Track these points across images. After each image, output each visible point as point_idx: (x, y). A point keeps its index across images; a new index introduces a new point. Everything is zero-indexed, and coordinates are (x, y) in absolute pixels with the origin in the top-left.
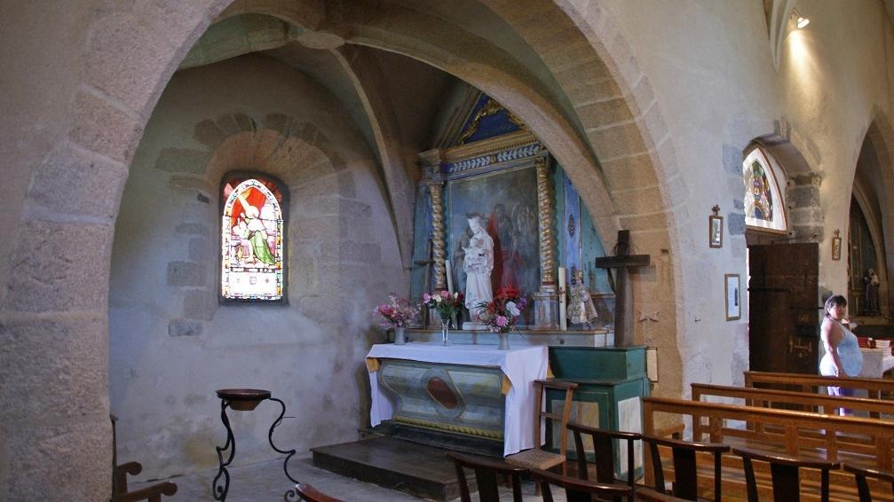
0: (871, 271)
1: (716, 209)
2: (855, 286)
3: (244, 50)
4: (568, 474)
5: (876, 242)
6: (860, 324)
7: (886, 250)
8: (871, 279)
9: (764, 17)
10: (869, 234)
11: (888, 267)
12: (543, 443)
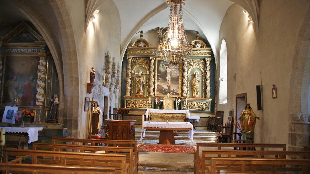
0: (55, 95)
1: (274, 86)
2: (47, 104)
3: (56, 63)
4: (37, 149)
5: (60, 79)
6: (45, 128)
7: (65, 84)
8: (54, 100)
9: (84, 17)
10: (57, 75)
11: (65, 94)
12: (90, 152)
